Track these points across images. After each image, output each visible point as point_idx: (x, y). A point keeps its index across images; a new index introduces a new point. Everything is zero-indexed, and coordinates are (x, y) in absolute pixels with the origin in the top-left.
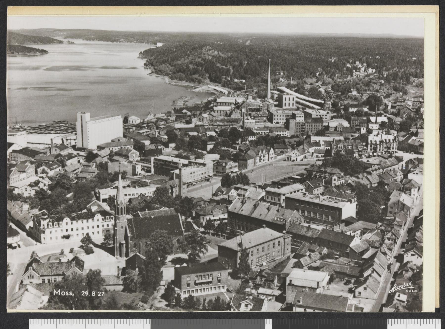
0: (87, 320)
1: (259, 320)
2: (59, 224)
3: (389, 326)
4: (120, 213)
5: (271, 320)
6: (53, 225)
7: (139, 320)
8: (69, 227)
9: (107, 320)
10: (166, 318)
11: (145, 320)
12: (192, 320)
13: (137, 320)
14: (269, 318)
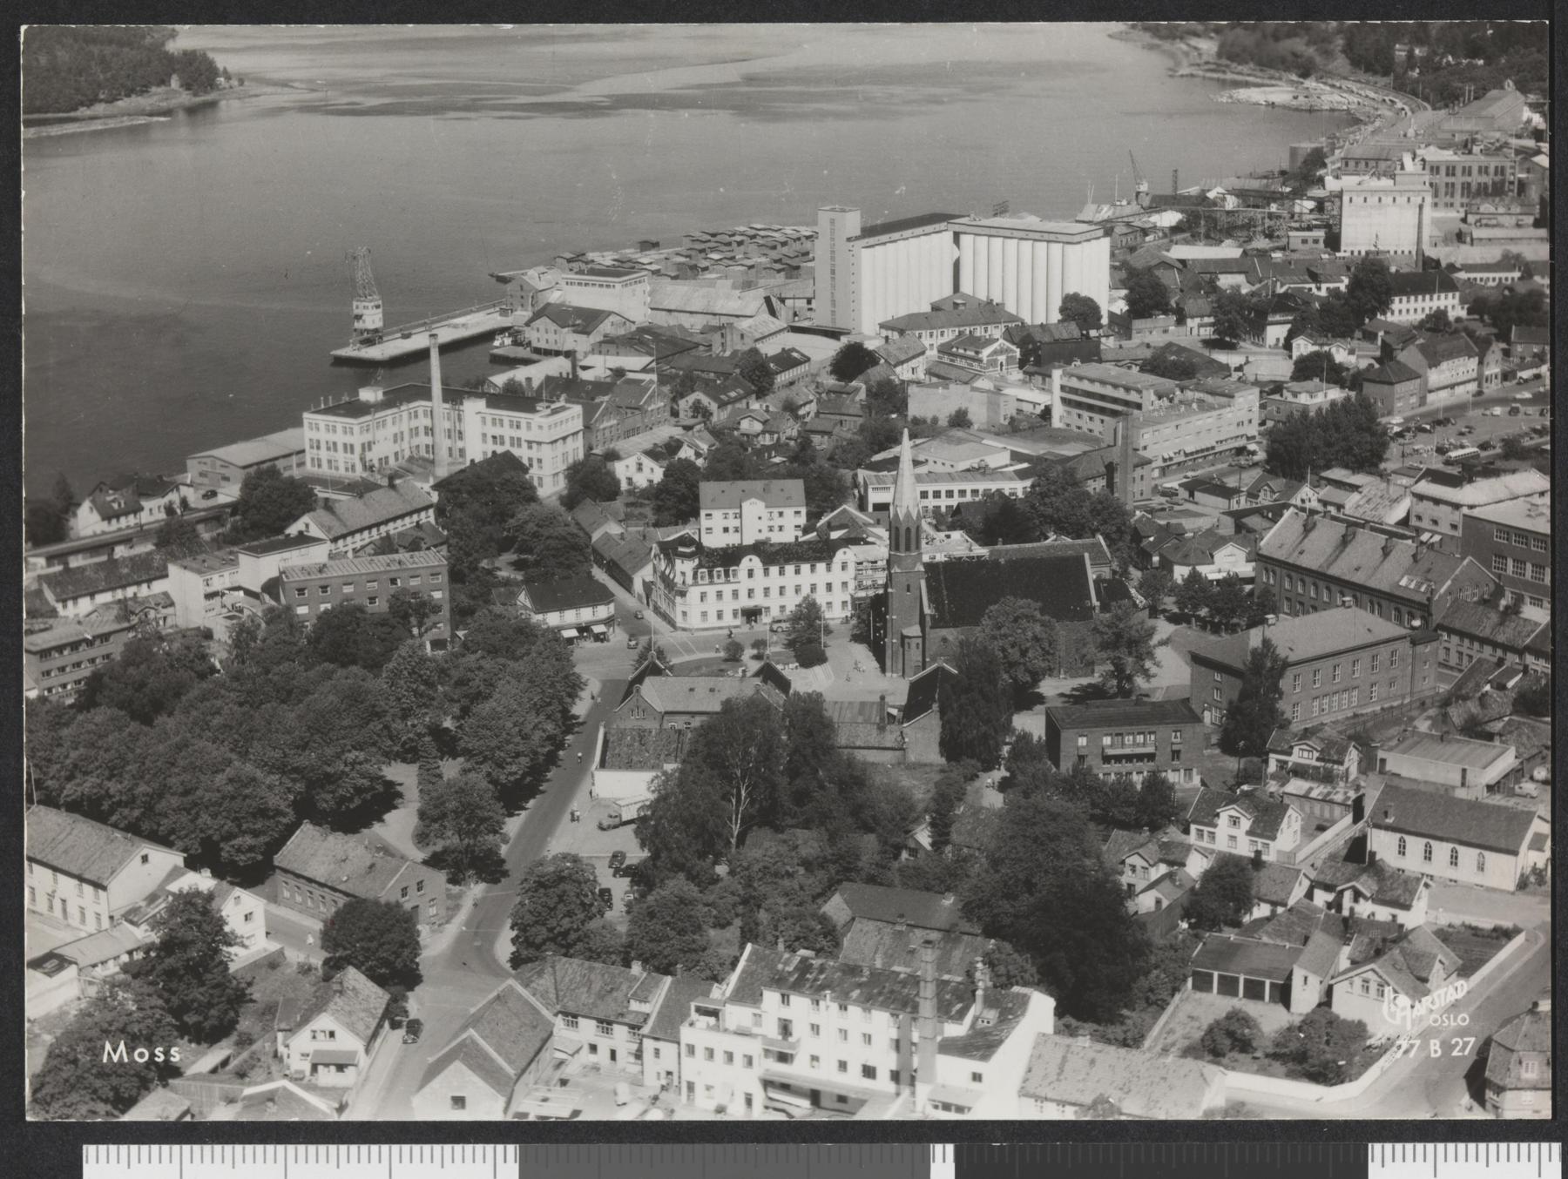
0: (291, 1148)
1: (907, 1147)
2: (727, 575)
3: (1374, 1169)
4: (902, 546)
5: (950, 1148)
6: (711, 576)
7: (479, 1147)
8: (760, 581)
9: (364, 1148)
10: (573, 1142)
11: (500, 1147)
12: (668, 1147)
13: (469, 1147)
14: (943, 1140)
